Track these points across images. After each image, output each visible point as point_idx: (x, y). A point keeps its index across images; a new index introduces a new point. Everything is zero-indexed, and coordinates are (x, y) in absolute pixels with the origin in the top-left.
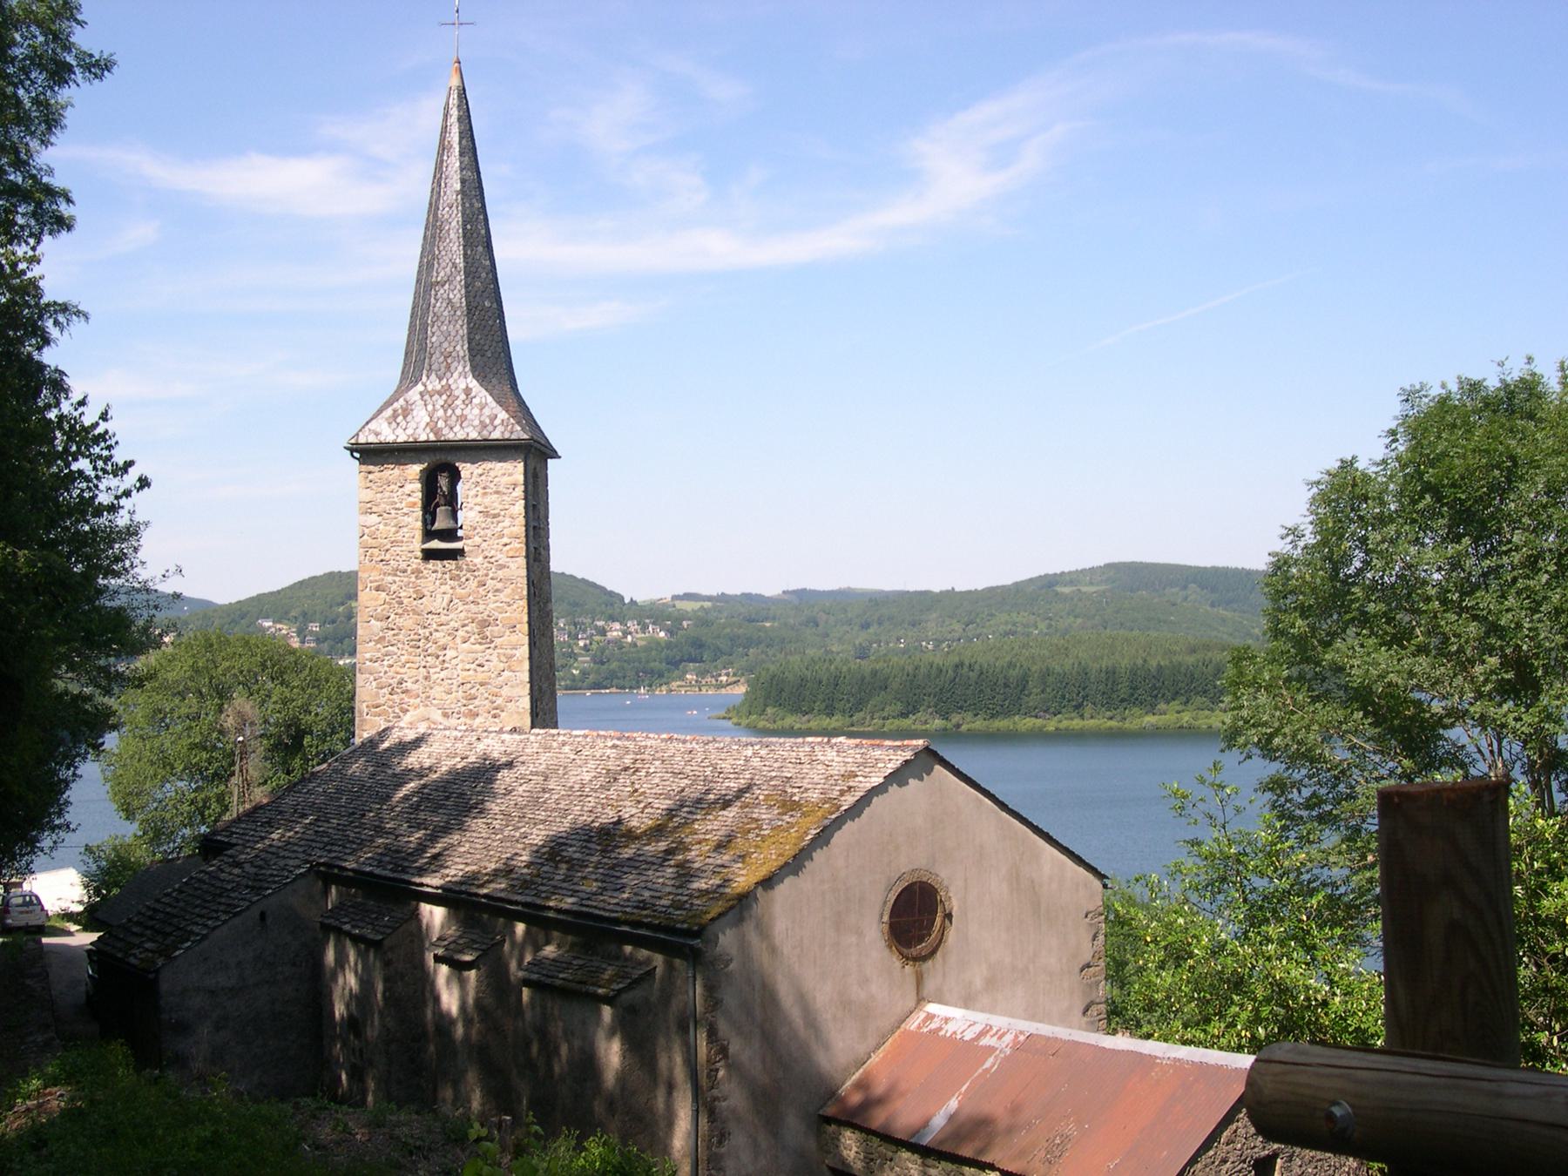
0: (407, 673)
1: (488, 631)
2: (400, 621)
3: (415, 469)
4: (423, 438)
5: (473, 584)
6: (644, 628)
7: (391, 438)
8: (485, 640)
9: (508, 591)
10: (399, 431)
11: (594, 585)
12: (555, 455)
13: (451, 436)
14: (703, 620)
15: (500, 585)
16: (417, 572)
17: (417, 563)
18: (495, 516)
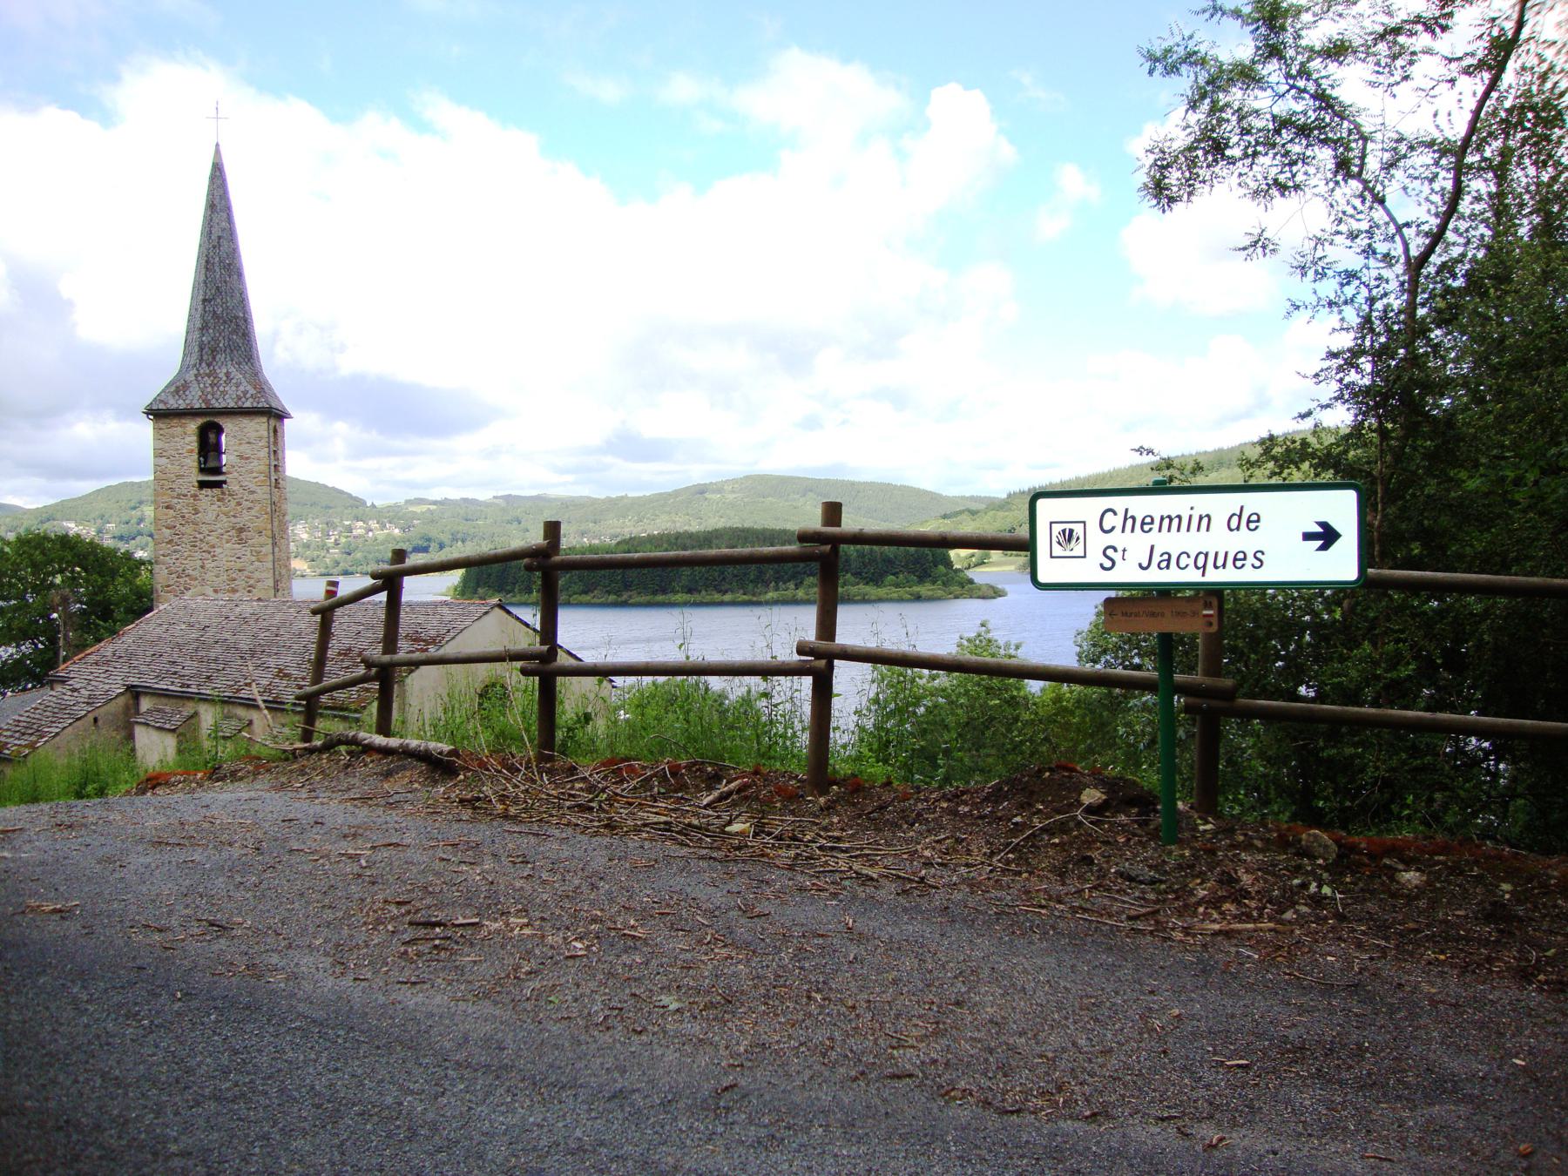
0: (189, 564)
1: (243, 535)
2: (183, 529)
3: (193, 426)
4: (197, 406)
5: (233, 503)
6: (383, 527)
7: (175, 406)
8: (241, 541)
9: (257, 508)
10: (181, 402)
11: (341, 492)
12: (289, 416)
13: (217, 405)
14: (431, 519)
15: (250, 505)
16: (195, 496)
17: (194, 490)
18: (247, 458)
